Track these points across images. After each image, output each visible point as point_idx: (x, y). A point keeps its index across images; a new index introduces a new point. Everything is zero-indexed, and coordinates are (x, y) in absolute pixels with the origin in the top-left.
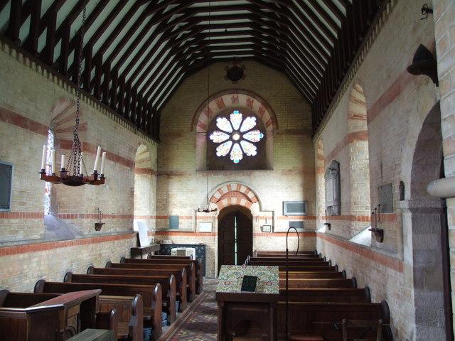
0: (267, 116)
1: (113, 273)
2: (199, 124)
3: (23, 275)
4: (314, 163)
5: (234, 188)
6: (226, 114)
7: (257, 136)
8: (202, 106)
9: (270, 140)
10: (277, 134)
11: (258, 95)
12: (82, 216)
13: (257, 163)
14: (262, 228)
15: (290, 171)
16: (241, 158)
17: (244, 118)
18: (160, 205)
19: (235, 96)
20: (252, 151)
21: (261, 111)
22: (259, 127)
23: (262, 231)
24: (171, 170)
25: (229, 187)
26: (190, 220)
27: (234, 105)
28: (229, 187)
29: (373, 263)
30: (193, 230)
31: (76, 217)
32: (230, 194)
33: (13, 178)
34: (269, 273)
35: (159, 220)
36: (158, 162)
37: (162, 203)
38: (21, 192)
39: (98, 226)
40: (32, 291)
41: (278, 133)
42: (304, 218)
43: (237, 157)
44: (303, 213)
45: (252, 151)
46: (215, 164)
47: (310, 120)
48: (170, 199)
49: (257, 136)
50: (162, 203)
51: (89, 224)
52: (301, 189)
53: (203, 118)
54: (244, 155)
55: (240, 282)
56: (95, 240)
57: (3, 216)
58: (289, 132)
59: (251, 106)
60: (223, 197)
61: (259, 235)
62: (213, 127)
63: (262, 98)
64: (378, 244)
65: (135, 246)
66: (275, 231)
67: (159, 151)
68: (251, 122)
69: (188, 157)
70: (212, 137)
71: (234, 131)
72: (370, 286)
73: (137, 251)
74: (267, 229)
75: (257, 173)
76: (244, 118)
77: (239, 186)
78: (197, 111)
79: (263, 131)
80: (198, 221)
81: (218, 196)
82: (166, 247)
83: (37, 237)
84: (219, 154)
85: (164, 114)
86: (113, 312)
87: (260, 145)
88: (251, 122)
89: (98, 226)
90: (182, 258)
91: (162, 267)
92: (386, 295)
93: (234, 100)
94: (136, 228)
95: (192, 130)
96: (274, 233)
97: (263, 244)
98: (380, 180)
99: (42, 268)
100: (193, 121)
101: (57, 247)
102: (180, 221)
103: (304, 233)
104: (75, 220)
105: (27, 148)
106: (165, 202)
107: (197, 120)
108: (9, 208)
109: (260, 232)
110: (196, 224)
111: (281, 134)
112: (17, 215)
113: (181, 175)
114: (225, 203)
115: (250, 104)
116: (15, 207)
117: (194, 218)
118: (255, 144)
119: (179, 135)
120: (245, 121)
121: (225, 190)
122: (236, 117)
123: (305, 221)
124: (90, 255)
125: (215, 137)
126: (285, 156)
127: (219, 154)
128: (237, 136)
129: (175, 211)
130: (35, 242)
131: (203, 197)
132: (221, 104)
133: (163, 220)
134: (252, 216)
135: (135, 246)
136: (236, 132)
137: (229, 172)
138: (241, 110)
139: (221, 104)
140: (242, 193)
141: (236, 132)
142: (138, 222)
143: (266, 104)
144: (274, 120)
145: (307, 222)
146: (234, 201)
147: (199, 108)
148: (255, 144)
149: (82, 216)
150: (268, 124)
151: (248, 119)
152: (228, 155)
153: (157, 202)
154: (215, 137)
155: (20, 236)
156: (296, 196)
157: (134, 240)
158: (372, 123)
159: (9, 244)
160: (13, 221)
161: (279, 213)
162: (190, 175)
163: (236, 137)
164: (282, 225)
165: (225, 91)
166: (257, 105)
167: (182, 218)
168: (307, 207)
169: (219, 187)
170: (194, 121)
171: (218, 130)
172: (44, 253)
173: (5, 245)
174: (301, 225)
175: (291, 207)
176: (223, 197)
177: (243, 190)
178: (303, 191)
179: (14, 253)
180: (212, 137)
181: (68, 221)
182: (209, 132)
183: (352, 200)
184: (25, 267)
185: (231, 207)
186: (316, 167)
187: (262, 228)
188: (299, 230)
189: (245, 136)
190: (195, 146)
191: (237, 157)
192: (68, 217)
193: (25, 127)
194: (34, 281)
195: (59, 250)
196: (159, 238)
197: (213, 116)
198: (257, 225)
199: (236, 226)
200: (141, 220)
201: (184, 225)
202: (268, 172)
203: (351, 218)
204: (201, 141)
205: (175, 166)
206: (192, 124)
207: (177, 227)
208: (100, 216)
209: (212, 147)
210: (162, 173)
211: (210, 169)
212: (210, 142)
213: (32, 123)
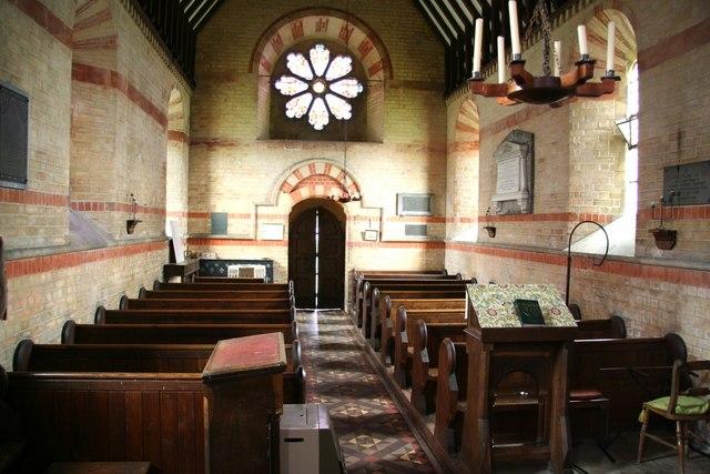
0: (375, 56)
1: (169, 307)
2: (262, 61)
3: (47, 313)
4: (446, 136)
5: (320, 169)
6: (304, 49)
7: (353, 88)
8: (269, 31)
9: (377, 99)
10: (391, 87)
11: (362, 22)
12: (111, 206)
13: (354, 131)
14: (363, 234)
15: (410, 146)
16: (326, 121)
17: (332, 57)
18: (194, 193)
19: (324, 19)
20: (343, 111)
21: (364, 49)
22: (356, 73)
23: (364, 239)
24: (213, 136)
25: (312, 167)
26: (246, 221)
27: (321, 35)
28: (312, 167)
29: (635, 281)
30: (252, 237)
31: (101, 208)
32: (313, 178)
33: (31, 123)
34: (653, 301)
35: (193, 220)
36: (191, 122)
37: (198, 190)
38: (39, 152)
39: (131, 224)
40: (59, 341)
41: (392, 85)
42: (429, 221)
43: (319, 120)
44: (426, 213)
45: (343, 111)
46: (285, 130)
47: (443, 69)
48: (212, 185)
49: (353, 88)
50: (198, 190)
51: (120, 218)
52: (425, 175)
53: (269, 53)
54: (332, 117)
55: (511, 312)
56: (130, 251)
57: (17, 197)
58: (409, 85)
59: (347, 38)
60: (302, 182)
61: (359, 245)
62: (281, 70)
63: (367, 25)
64: (658, 252)
65: (167, 262)
66: (384, 239)
67: (193, 103)
68: (343, 65)
69: (242, 117)
70: (278, 85)
71: (323, 77)
72: (625, 315)
73: (171, 269)
74: (372, 236)
75: (358, 147)
76: (332, 57)
77: (328, 167)
78: (260, 39)
79: (363, 80)
80: (260, 221)
81: (293, 181)
82: (207, 265)
83: (60, 241)
84: (290, 114)
85: (202, 40)
86: (304, 373)
87: (357, 103)
88: (343, 65)
89: (131, 224)
90: (249, 280)
91: (237, 296)
92: (678, 327)
93: (321, 27)
94: (169, 234)
95: (250, 71)
96: (379, 246)
97: (362, 258)
98: (674, 157)
99: (70, 299)
100: (253, 55)
101: (85, 262)
102: (230, 221)
103: (427, 243)
104: (99, 214)
105: (45, 68)
106: (203, 190)
107: (260, 54)
108: (25, 181)
109: (359, 239)
110: (256, 226)
111: (397, 87)
112: (36, 198)
113: (231, 145)
114: (305, 193)
115: (346, 34)
116: (34, 185)
117: (253, 217)
118: (350, 101)
119: (229, 77)
120: (333, 63)
121: (306, 173)
122: (320, 55)
123: (429, 224)
124: (122, 276)
125: (285, 85)
126: (400, 122)
127: (290, 114)
128: (319, 86)
129: (220, 205)
130: (57, 250)
131: (268, 182)
132: (298, 32)
133: (201, 220)
134: (345, 216)
135: (167, 262)
136: (319, 79)
137: (312, 144)
138: (328, 44)
139: (298, 32)
140: (332, 178)
141: (319, 79)
142: (171, 222)
143: (374, 36)
144: (387, 63)
145: (434, 228)
146: (320, 191)
147: (263, 35)
148: (350, 101)
149: (111, 206)
150: (374, 70)
151: (339, 59)
152: (306, 117)
153: (189, 189)
154: (285, 85)
155: (40, 241)
156: (417, 185)
157: (167, 251)
158: (648, 72)
159: (30, 253)
160: (31, 208)
161: (390, 211)
162: (247, 145)
163: (319, 88)
164: (395, 230)
165: (308, 8)
166: (358, 36)
167: (233, 216)
168: (435, 204)
169: (297, 167)
170: (255, 56)
171: (289, 73)
172: (70, 272)
173: (26, 254)
174: (424, 231)
175: (409, 203)
176: (302, 182)
177: (335, 173)
178: (429, 179)
179: (34, 272)
180: (278, 85)
181: (88, 215)
182: (275, 78)
183: (572, 189)
184: (49, 297)
185: (312, 200)
186: (449, 143)
187: (363, 234)
188: (420, 238)
189: (332, 87)
190: (256, 99)
191: (319, 120)
192: (88, 207)
193: (41, 23)
194: (61, 322)
195: (88, 267)
196: (194, 249)
197: (283, 50)
198: (353, 231)
199: (317, 228)
200: (174, 219)
201: (235, 228)
202: (375, 146)
203: (566, 217)
204: (264, 91)
205: (223, 129)
206: (252, 60)
207: (225, 231)
208: (134, 208)
209: (279, 101)
210: (200, 142)
211: (272, 138)
212: (275, 93)
213: (52, 18)
